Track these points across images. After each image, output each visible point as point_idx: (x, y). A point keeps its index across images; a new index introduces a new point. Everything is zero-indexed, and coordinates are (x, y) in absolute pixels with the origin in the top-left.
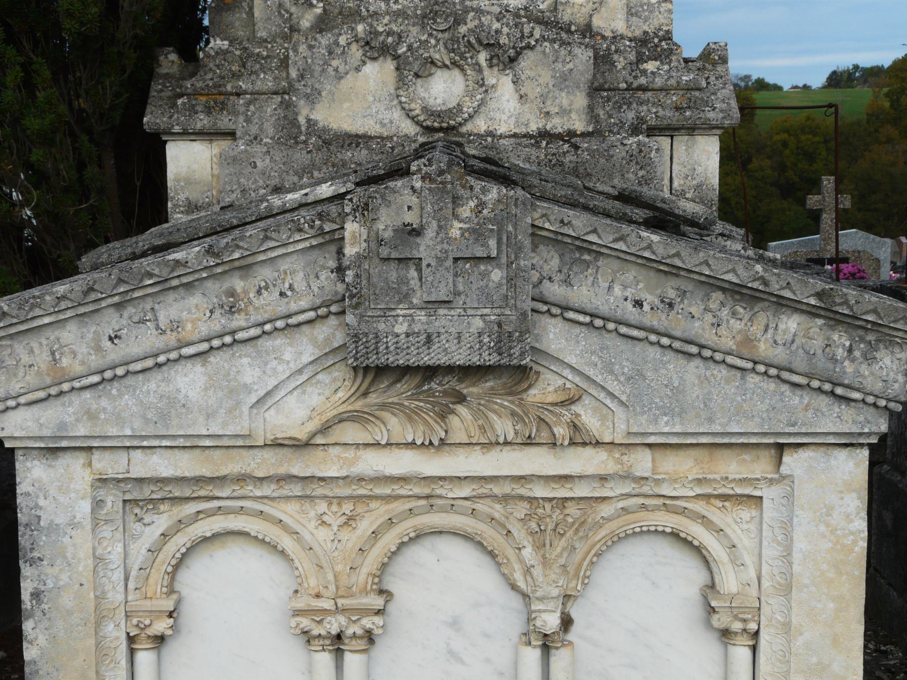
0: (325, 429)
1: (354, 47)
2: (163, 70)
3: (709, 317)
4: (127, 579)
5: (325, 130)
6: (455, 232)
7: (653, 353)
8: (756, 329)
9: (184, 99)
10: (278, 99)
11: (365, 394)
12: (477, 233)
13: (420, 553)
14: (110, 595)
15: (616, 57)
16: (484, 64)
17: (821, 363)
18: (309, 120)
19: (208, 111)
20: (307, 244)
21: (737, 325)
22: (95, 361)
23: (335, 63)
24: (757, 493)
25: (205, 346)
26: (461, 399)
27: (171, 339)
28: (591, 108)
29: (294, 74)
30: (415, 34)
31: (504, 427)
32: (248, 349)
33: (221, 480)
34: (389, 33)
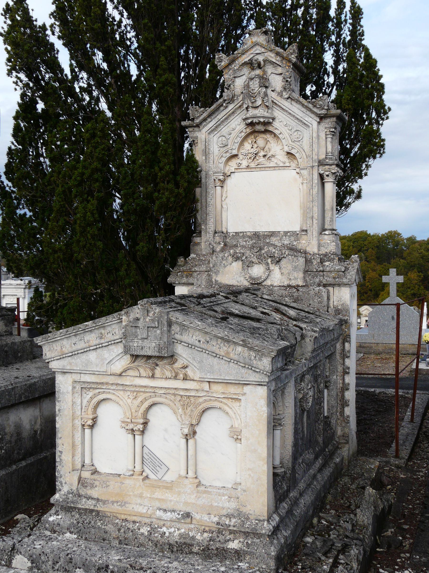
0: (125, 371)
1: (230, 257)
2: (179, 264)
3: (218, 346)
4: (82, 409)
5: (220, 283)
6: (147, 320)
7: (205, 355)
8: (230, 350)
9: (180, 273)
10: (207, 273)
11: (134, 362)
12: (153, 320)
13: (155, 409)
14: (77, 412)
15: (313, 261)
16: (270, 263)
17: (247, 360)
18: (215, 280)
19: (187, 277)
20: (117, 322)
21: (225, 348)
22: (70, 350)
23: (224, 262)
24: (239, 398)
25: (95, 347)
26: (157, 365)
27: (87, 345)
28: (304, 277)
29: (211, 265)
30: (248, 253)
31: (168, 374)
32: (106, 348)
33: (102, 383)
34: (240, 253)
